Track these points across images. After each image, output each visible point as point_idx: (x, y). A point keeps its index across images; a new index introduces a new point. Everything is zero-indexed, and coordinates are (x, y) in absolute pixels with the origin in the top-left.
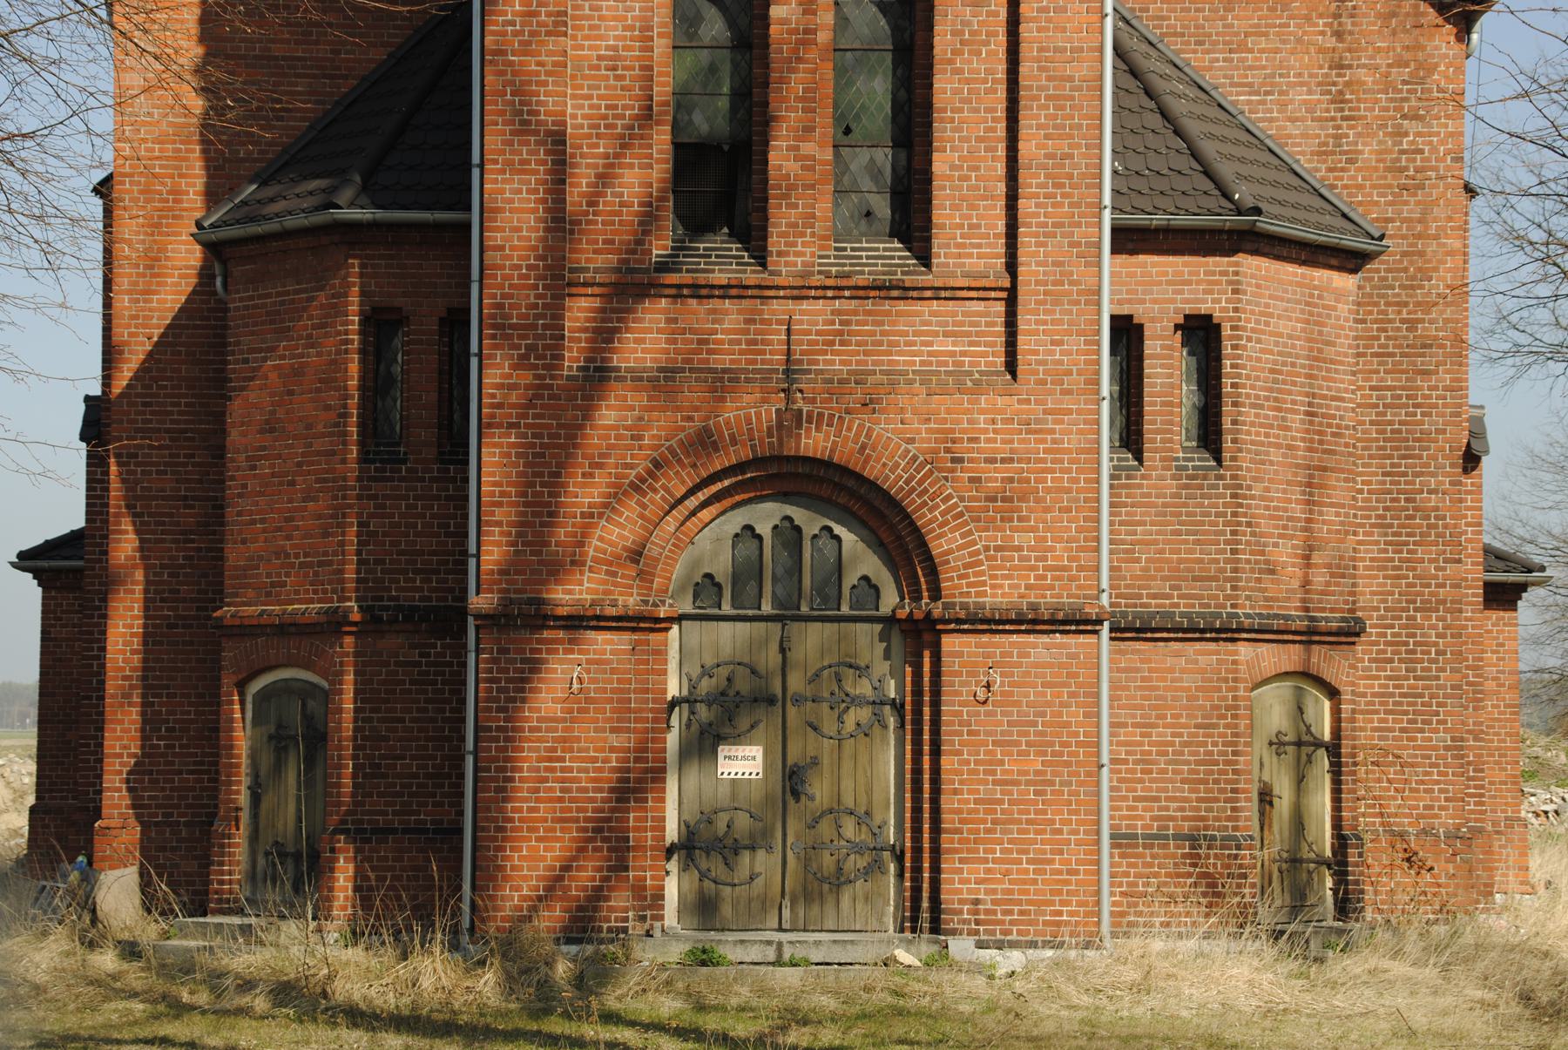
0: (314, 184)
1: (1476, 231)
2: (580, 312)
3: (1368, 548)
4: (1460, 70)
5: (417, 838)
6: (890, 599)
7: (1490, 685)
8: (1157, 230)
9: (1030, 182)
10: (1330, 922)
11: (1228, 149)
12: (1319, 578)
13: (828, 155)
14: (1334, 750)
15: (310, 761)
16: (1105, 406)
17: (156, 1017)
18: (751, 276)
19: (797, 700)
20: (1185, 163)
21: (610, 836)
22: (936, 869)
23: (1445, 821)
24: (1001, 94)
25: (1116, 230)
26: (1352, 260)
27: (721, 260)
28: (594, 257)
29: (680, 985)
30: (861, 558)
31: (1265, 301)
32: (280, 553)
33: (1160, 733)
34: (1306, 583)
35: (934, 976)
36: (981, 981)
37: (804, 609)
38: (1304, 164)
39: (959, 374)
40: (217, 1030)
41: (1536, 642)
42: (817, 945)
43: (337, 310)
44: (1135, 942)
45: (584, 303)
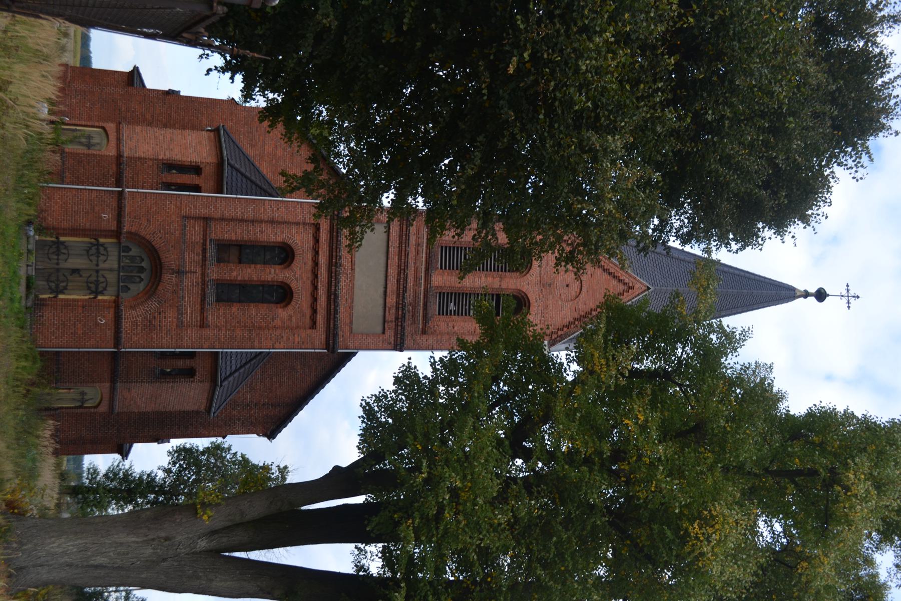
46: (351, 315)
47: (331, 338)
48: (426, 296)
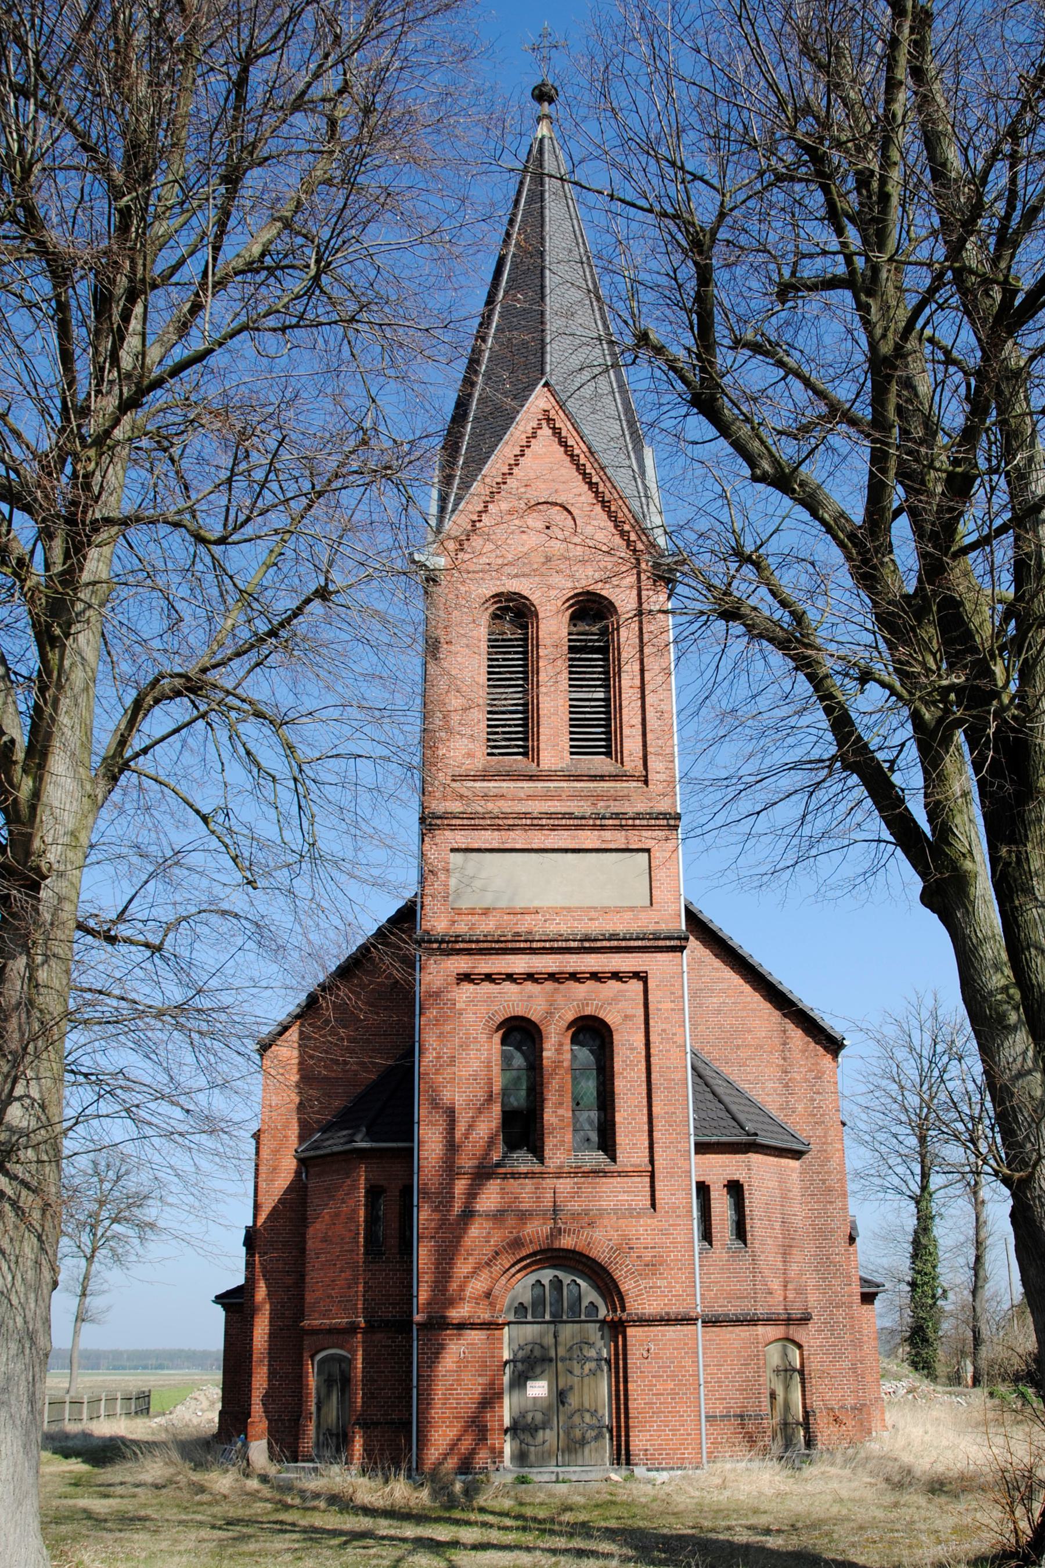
0: (345, 1133)
1: (847, 1142)
2: (461, 1186)
3: (811, 1280)
4: (835, 1073)
5: (391, 1431)
6: (603, 1312)
7: (866, 1338)
8: (714, 1144)
9: (658, 1125)
10: (803, 1451)
11: (741, 1108)
12: (791, 1295)
13: (570, 1114)
14: (801, 1372)
15: (343, 1391)
16: (695, 1222)
17: (277, 1510)
18: (537, 1168)
19: (563, 1360)
20: (724, 1114)
21: (477, 1426)
22: (627, 1436)
23: (850, 1402)
24: (644, 1086)
25: (697, 1144)
26: (797, 1154)
27: (523, 1161)
28: (466, 1162)
29: (512, 1493)
30: (590, 1295)
31: (760, 1172)
32: (330, 1296)
33: (726, 1368)
34: (785, 1298)
35: (628, 1485)
36: (650, 1486)
37: (565, 1318)
38: (774, 1113)
39: (631, 1210)
40: (304, 1517)
41: (881, 1316)
42: (573, 1472)
43: (355, 1187)
44: (719, 1465)
45: (463, 1182)
46: (618, 910)
47: (661, 943)
48: (578, 778)
